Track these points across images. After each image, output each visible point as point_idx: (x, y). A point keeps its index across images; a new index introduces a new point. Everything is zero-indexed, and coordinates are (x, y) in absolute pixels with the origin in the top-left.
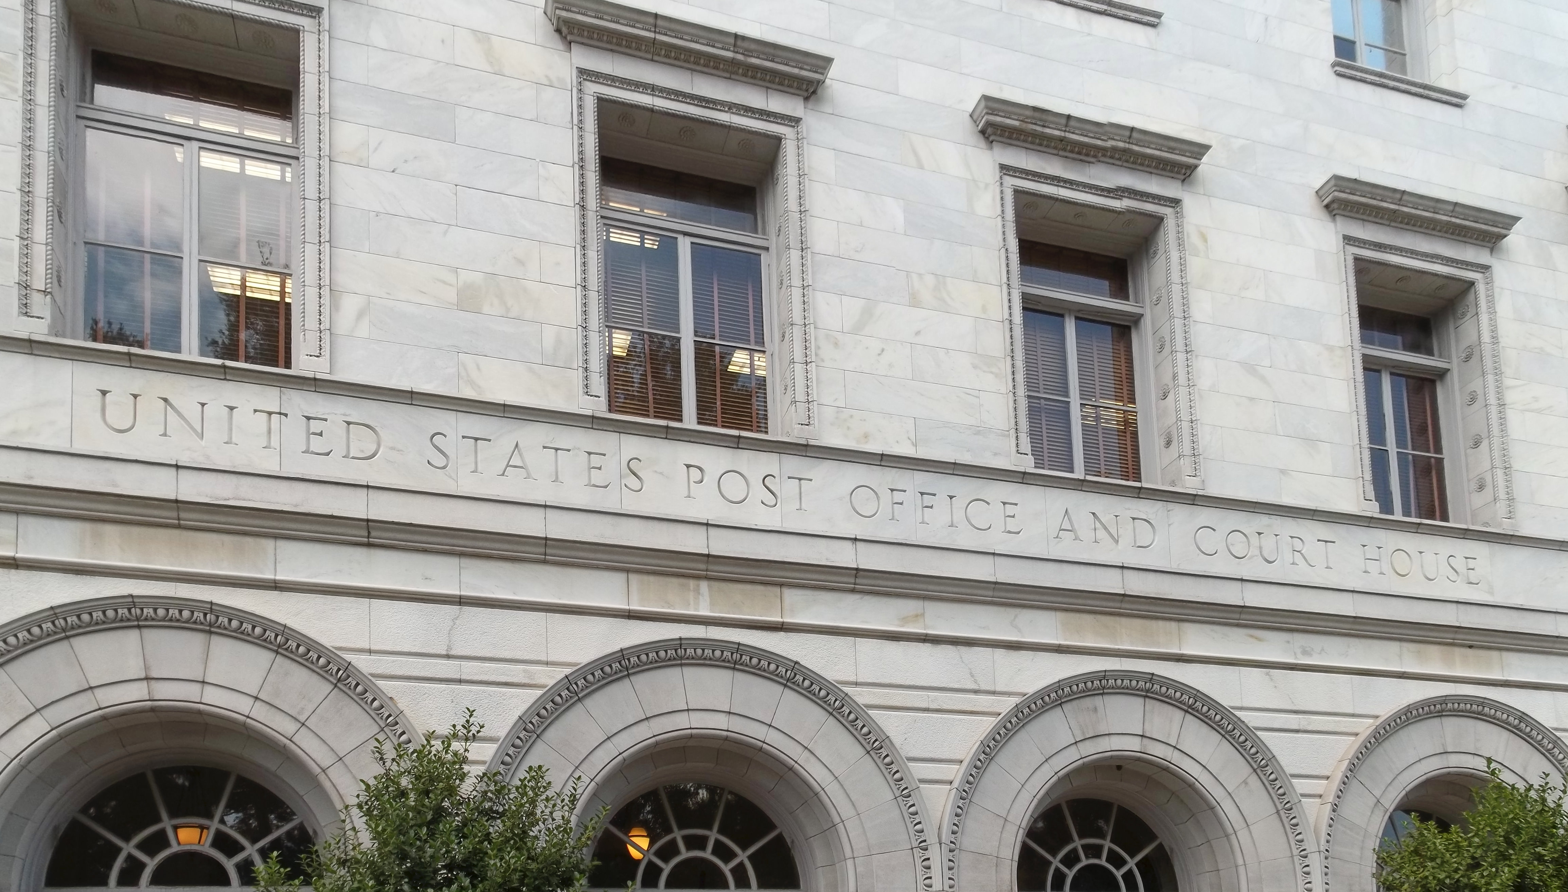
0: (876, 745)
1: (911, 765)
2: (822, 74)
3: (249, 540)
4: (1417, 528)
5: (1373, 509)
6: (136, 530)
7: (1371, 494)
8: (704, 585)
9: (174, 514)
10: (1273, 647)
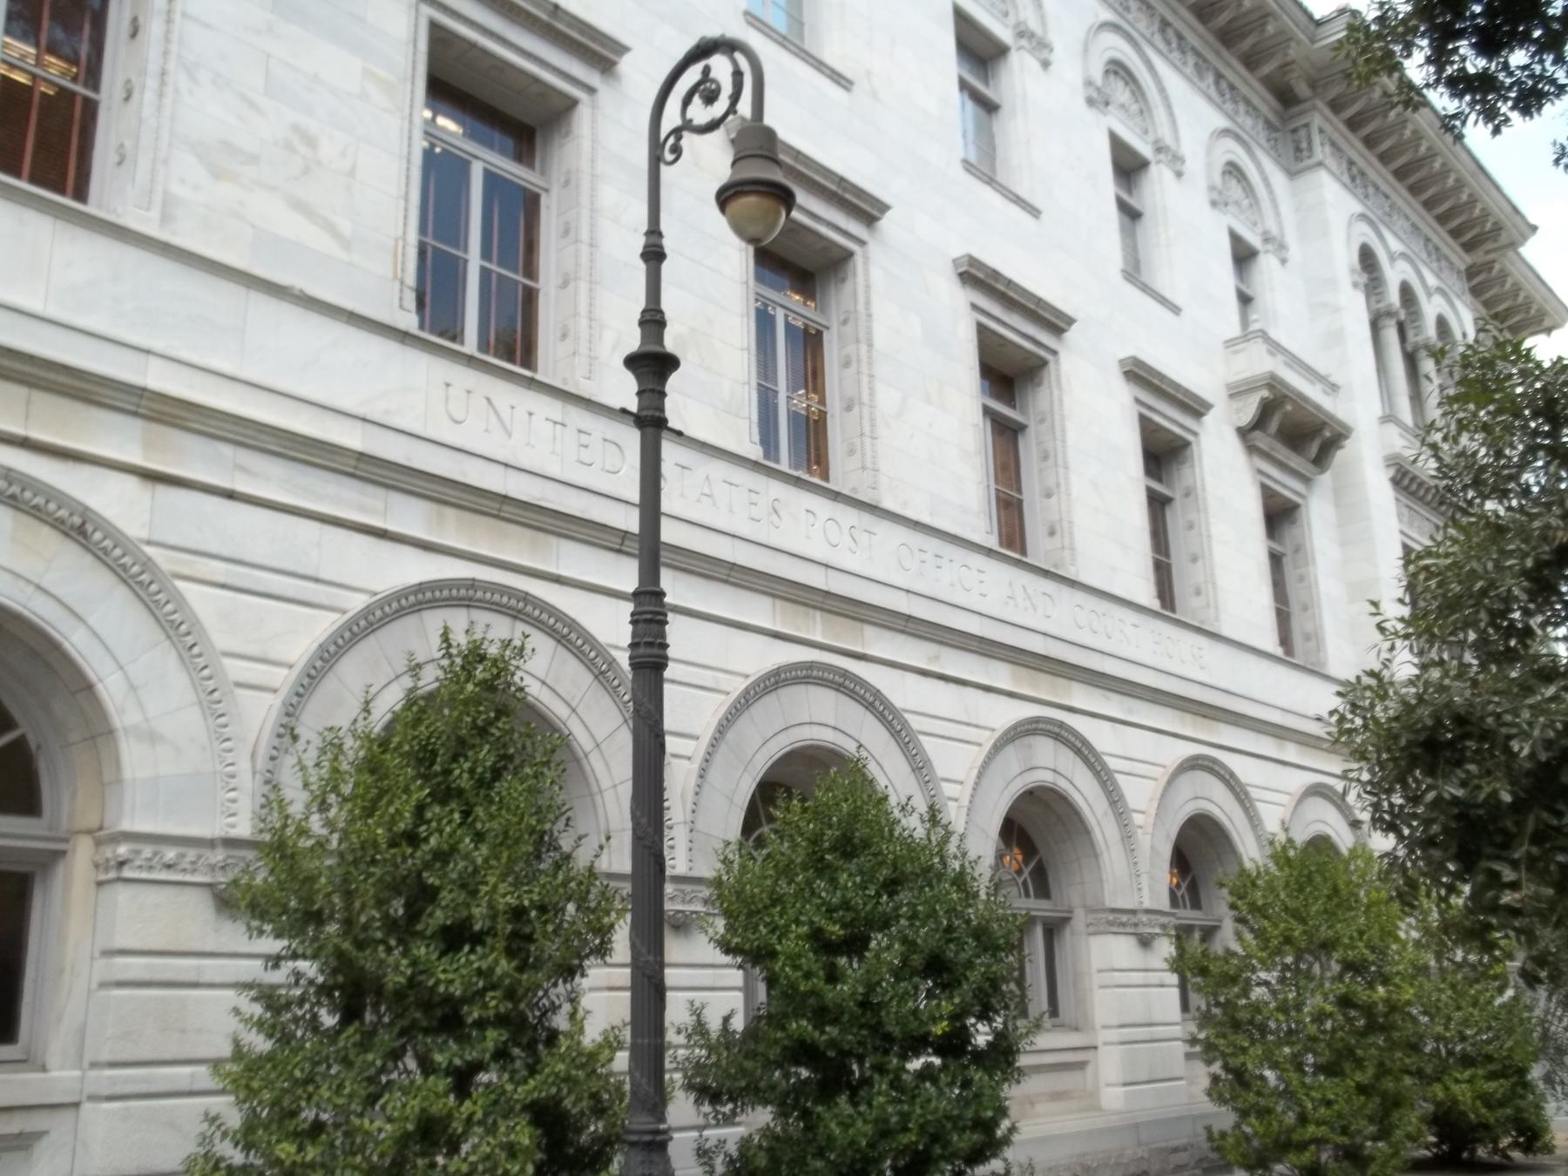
0: (177, 628)
1: (227, 661)
2: (1306, 480)
3: (541, 535)
4: (798, 482)
5: (755, 452)
6: (467, 515)
7: (756, 438)
8: (818, 614)
9: (497, 506)
10: (1266, 745)
